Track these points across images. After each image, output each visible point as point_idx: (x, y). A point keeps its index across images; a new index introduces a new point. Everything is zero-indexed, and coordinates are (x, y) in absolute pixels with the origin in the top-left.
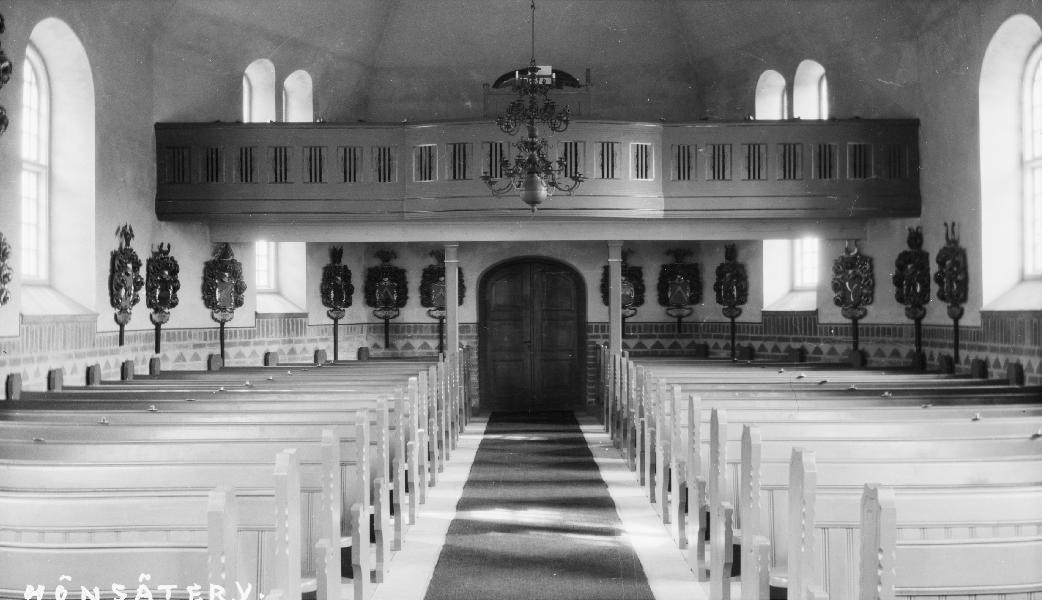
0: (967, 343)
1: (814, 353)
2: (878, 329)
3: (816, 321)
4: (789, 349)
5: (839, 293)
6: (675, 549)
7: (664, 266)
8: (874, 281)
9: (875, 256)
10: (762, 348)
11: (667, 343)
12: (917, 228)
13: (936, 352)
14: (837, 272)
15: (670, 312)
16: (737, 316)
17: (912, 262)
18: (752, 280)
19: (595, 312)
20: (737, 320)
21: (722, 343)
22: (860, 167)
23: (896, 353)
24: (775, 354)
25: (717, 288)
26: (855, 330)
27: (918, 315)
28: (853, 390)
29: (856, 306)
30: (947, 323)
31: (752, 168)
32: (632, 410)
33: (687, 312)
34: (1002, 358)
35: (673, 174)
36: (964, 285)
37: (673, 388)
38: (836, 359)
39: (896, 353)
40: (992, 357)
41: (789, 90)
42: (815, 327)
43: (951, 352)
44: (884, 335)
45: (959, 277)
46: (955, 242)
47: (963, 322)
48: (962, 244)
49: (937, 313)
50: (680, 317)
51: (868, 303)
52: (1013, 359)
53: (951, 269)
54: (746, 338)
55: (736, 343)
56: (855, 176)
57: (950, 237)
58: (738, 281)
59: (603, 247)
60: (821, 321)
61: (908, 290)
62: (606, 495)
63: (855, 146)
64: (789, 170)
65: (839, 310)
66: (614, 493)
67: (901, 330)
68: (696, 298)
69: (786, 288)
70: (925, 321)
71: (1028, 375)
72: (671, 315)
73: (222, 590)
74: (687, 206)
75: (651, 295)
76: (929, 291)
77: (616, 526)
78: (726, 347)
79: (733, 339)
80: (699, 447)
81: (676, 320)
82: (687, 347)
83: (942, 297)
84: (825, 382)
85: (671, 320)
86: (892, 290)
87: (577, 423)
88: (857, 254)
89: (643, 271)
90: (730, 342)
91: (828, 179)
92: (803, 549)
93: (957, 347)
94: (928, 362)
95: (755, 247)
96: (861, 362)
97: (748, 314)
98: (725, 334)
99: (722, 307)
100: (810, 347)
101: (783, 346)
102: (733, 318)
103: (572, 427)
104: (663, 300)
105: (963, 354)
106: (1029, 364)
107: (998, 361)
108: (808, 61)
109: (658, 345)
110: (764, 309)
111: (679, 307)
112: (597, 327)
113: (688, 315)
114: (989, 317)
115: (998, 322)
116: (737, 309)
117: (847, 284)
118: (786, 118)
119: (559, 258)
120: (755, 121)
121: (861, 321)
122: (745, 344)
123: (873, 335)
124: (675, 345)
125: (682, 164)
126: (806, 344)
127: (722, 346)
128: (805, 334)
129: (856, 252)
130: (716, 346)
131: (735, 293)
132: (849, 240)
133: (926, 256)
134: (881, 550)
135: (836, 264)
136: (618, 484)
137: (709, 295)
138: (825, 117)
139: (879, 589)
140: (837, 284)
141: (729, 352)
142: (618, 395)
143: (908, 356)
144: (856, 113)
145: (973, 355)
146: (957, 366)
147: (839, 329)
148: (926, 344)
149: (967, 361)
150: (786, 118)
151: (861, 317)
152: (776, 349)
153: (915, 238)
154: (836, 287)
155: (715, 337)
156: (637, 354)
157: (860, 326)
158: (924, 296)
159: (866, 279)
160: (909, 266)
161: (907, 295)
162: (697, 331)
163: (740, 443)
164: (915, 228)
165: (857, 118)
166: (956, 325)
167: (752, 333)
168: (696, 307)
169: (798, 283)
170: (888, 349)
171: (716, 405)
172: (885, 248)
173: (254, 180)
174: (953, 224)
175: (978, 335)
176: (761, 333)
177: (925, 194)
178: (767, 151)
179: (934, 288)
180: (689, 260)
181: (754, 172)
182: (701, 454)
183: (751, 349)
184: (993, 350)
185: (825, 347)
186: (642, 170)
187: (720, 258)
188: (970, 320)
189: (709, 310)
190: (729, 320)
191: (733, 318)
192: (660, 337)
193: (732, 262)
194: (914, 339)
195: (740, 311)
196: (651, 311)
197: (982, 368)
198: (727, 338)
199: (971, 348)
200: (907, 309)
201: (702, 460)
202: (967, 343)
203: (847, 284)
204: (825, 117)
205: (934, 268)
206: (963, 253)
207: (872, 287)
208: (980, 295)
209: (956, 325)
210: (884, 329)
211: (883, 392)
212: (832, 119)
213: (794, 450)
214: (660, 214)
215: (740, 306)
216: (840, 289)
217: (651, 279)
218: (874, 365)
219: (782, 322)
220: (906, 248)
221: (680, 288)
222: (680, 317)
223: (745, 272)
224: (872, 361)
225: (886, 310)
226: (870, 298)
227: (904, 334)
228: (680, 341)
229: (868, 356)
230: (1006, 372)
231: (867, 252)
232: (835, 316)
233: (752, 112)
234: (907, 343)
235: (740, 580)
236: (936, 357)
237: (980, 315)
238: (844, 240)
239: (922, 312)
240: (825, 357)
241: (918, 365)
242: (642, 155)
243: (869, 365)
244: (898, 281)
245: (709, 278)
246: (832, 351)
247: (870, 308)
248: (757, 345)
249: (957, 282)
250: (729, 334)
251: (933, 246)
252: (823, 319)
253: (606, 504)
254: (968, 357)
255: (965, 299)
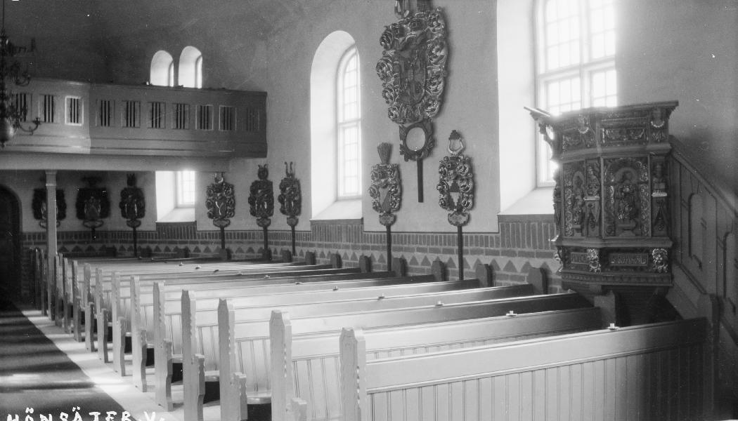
0: (301, 242)
1: (194, 251)
2: (238, 234)
3: (195, 229)
4: (177, 249)
5: (212, 209)
6: (139, 393)
7: (80, 190)
8: (234, 200)
9: (234, 184)
10: (157, 249)
11: (84, 247)
12: (265, 165)
13: (279, 248)
14: (209, 195)
15: (87, 224)
16: (138, 226)
17: (260, 192)
18: (148, 199)
19: (29, 224)
20: (138, 229)
21: (126, 246)
22: (228, 121)
23: (251, 250)
24: (196, 253)
25: (122, 206)
26: (222, 235)
27: (265, 224)
28: (240, 275)
29: (222, 218)
30: (287, 229)
31: (129, 118)
32: (78, 297)
33: (99, 223)
34: (326, 251)
35: (97, 120)
36: (298, 204)
37: (133, 278)
38: (209, 255)
39: (251, 250)
40: (319, 251)
41: (176, 63)
42: (195, 233)
43: (290, 248)
44: (242, 238)
45: (296, 199)
46: (292, 175)
47: (298, 228)
48: (297, 176)
49: (279, 222)
50: (93, 228)
51: (231, 216)
52: (334, 251)
53: (290, 193)
54: (145, 242)
55: (138, 245)
56: (71, 121)
57: (289, 172)
58: (137, 201)
59: (42, 176)
60: (198, 229)
61: (258, 207)
62: (67, 361)
63: (71, 99)
64: (180, 122)
65: (211, 221)
66: (75, 359)
67: (254, 234)
68: (106, 213)
69: (171, 205)
70: (269, 228)
71: (344, 261)
72: (87, 226)
73: (67, 416)
74: (108, 146)
75: (71, 211)
76: (273, 208)
77: (88, 381)
78: (130, 249)
79: (135, 243)
80: (164, 319)
81: (91, 230)
82: (100, 250)
83: (283, 212)
84: (217, 271)
85: (86, 229)
86: (248, 207)
87: (19, 310)
88: (223, 183)
89: (65, 193)
90: (133, 245)
91: (206, 130)
92: (286, 376)
93: (294, 244)
94: (273, 255)
95: (150, 177)
96: (228, 257)
97: (146, 225)
98: (129, 239)
99: (126, 220)
100: (192, 248)
101: (172, 247)
102: (134, 228)
103: (15, 313)
104: (80, 215)
105: (298, 249)
106: (346, 254)
107: (324, 253)
108: (191, 47)
109: (77, 249)
110: (500, 214)
111: (93, 220)
112: (29, 236)
113: (100, 226)
114: (315, 224)
115: (325, 229)
116: (137, 221)
117: (216, 203)
118: (172, 85)
119: (194, 182)
120: (151, 85)
121: (225, 229)
122: (144, 246)
123: (235, 238)
124: (90, 249)
125: (103, 114)
126: (188, 245)
127: (126, 249)
128: (188, 238)
129: (222, 181)
130: (122, 248)
131: (136, 210)
132: (217, 172)
133: (270, 184)
134: (358, 367)
135: (208, 189)
136: (75, 352)
137: (116, 212)
138: (200, 86)
139: (358, 391)
140: (209, 203)
141: (133, 252)
142: (60, 286)
143: (259, 252)
144: (223, 85)
145: (305, 250)
146: (294, 257)
147: (211, 235)
148: (271, 243)
149: (301, 254)
150: (172, 85)
151: (226, 226)
152: (167, 249)
153: (263, 172)
154: (209, 205)
155: (121, 242)
156: (71, 256)
157: (225, 232)
158: (270, 210)
159: (230, 199)
160: (259, 191)
161: (258, 210)
162: (106, 237)
163: (217, 312)
164: (263, 166)
165: (224, 89)
166: (293, 230)
167: (181, 238)
168: (106, 220)
169: (180, 203)
170: (245, 247)
171: (186, 287)
172: (243, 177)
173: (54, 121)
174: (291, 163)
175: (307, 235)
176: (156, 238)
177: (269, 143)
178: (165, 108)
179: (277, 205)
180: (100, 186)
181: (156, 123)
182: (165, 323)
183: (149, 250)
184: (320, 246)
185: (202, 247)
186: (74, 117)
187: (123, 184)
188: (303, 226)
189: (116, 221)
190: (131, 229)
191: (134, 228)
192: (79, 243)
193: (132, 187)
194: (263, 240)
195: (140, 223)
196: (72, 223)
197: (312, 258)
198: (131, 242)
199: (304, 245)
200: (258, 220)
201: (167, 329)
202: (301, 242)
203: (216, 203)
204: (200, 86)
205: (277, 192)
206: (297, 182)
207: (234, 205)
208: (155, 211)
209: (293, 230)
210: (242, 234)
211: (264, 275)
212: (203, 89)
213: (273, 312)
214: (87, 151)
215: (140, 219)
216: (211, 207)
217: (71, 200)
218: (236, 259)
219: (171, 230)
220: (257, 179)
221: (93, 206)
222: (93, 228)
223: (142, 194)
224: (234, 256)
225: (243, 221)
226: (232, 212)
227: (256, 236)
228: (94, 246)
229: (232, 252)
230: (329, 260)
231: (230, 181)
232: (208, 225)
233: (148, 78)
234: (258, 242)
235: (219, 404)
236: (279, 251)
237: (497, 218)
238: (214, 172)
239: (268, 222)
240: (202, 254)
241: (267, 257)
242: (74, 105)
243: (233, 259)
244: (251, 201)
245: (115, 198)
246: (207, 250)
247: (232, 220)
248: (153, 247)
249: (294, 201)
250: (132, 239)
251: (276, 178)
252: (200, 228)
253: (71, 367)
254: (302, 251)
255: (299, 213)
